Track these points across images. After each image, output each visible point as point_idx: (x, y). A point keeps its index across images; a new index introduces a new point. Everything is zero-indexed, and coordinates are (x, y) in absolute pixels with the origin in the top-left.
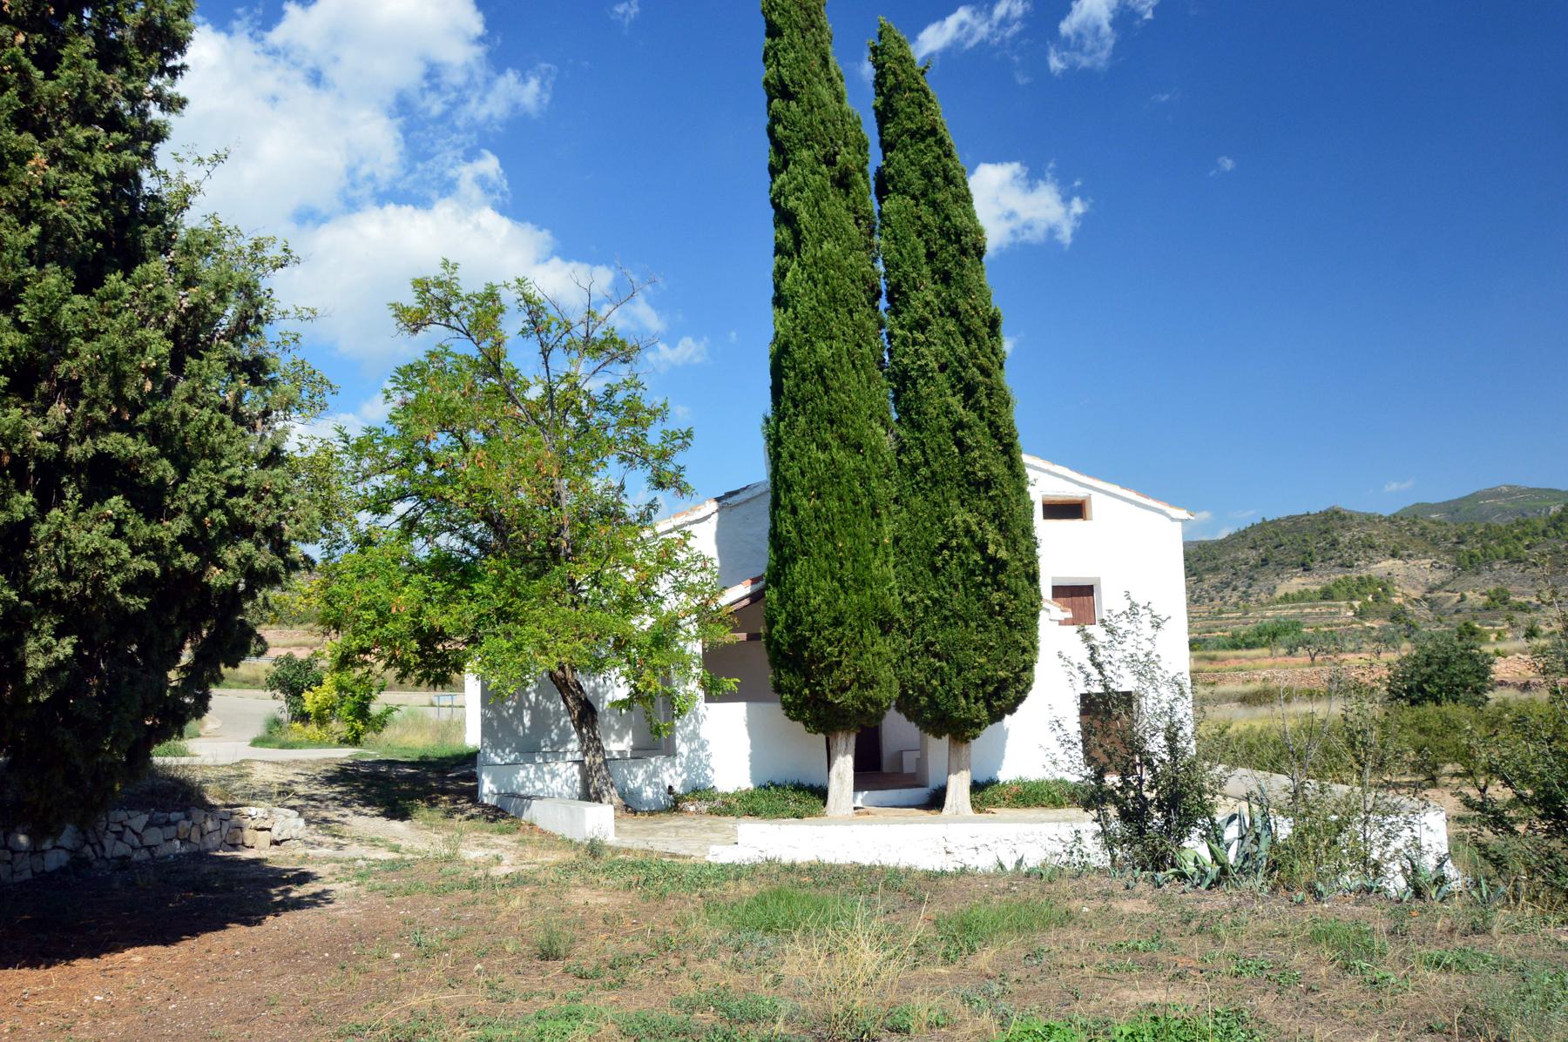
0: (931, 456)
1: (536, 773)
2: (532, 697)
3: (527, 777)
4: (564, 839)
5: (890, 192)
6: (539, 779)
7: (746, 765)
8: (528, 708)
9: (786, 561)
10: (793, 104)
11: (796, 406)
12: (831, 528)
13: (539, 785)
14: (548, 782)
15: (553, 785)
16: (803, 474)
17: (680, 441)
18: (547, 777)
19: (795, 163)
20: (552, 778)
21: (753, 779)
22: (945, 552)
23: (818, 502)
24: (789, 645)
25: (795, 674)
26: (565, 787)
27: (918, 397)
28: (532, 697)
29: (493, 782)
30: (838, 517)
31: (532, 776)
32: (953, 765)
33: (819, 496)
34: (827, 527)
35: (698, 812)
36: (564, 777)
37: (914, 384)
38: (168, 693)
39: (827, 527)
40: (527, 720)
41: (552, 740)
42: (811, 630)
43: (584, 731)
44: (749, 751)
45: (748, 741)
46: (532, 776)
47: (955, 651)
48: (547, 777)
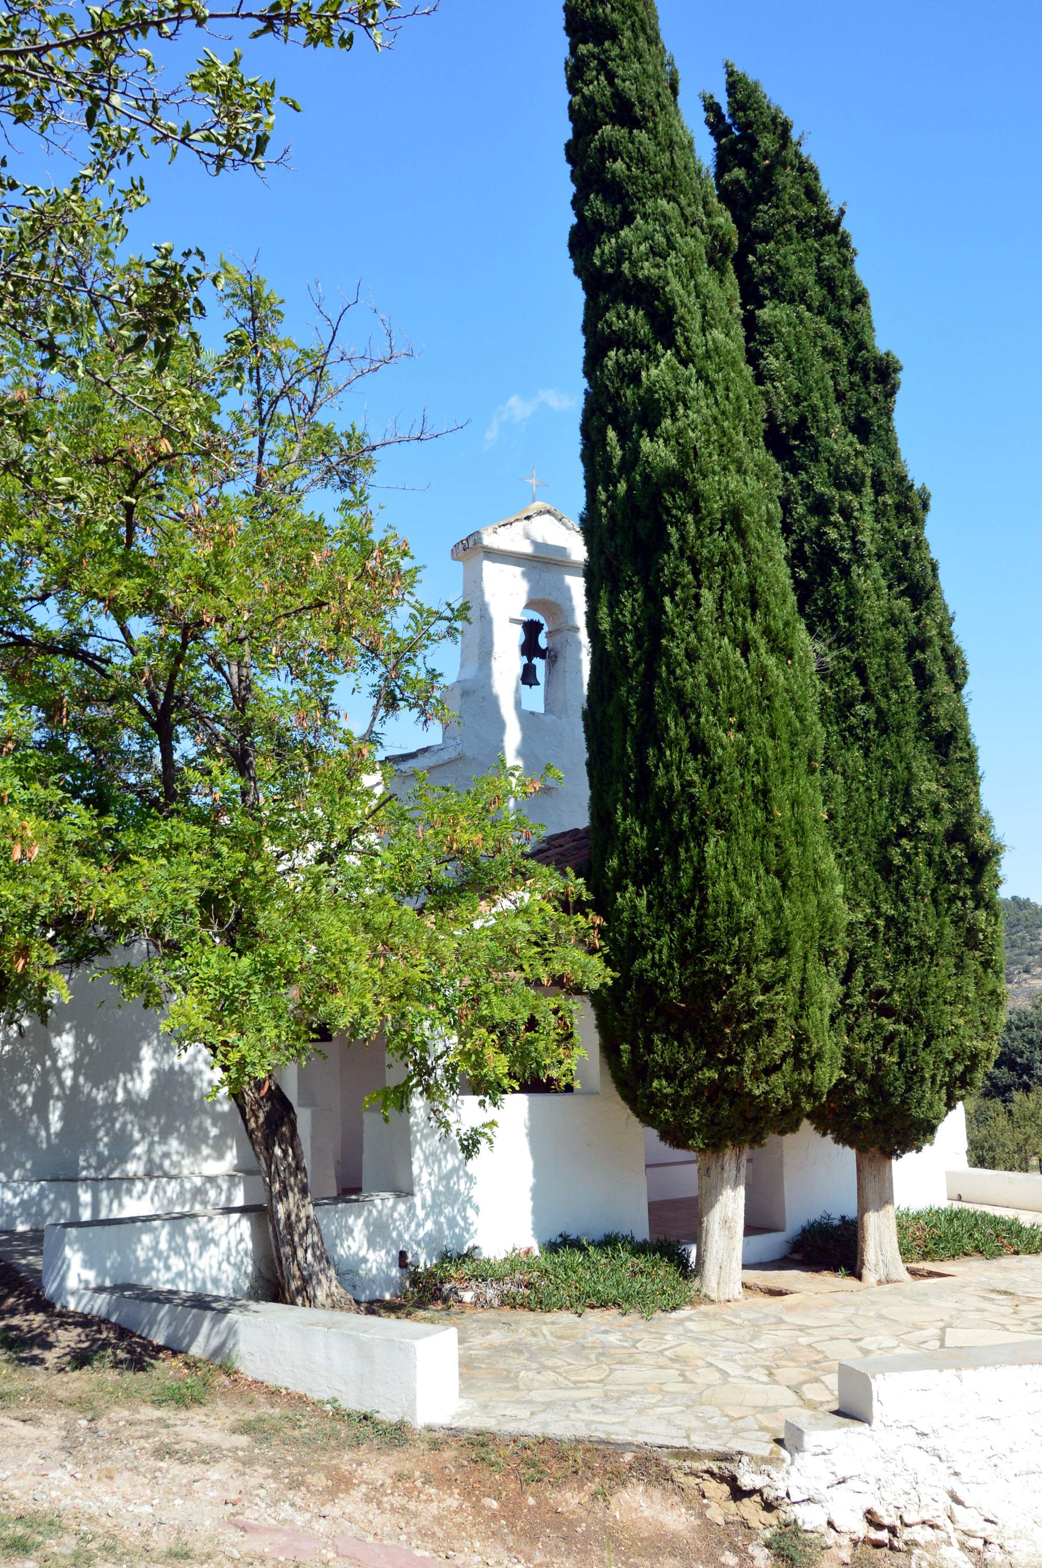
0: (875, 689)
1: (172, 1236)
2: (68, 1075)
3: (155, 1248)
4: (341, 1415)
5: (765, 298)
6: (177, 1250)
7: (526, 1205)
8: (58, 1098)
9: (679, 838)
10: (641, 135)
11: (696, 573)
12: (765, 784)
13: (177, 1263)
14: (194, 1257)
15: (202, 1264)
16: (712, 685)
17: (444, 625)
18: (193, 1246)
19: (645, 217)
20: (203, 1248)
21: (538, 1229)
22: (904, 841)
23: (740, 736)
24: (683, 990)
25: (682, 1043)
26: (225, 1266)
27: (852, 592)
28: (68, 1075)
29: (88, 1264)
30: (773, 766)
31: (163, 1245)
32: (870, 1194)
33: (740, 727)
34: (757, 780)
35: (485, 1305)
36: (223, 1246)
37: (846, 571)
38: (28, 1165)
39: (757, 780)
40: (55, 1122)
41: (100, 1155)
42: (736, 961)
43: (278, 1151)
44: (530, 1180)
45: (528, 1164)
46: (163, 1245)
47: (924, 1004)
48: (193, 1246)
